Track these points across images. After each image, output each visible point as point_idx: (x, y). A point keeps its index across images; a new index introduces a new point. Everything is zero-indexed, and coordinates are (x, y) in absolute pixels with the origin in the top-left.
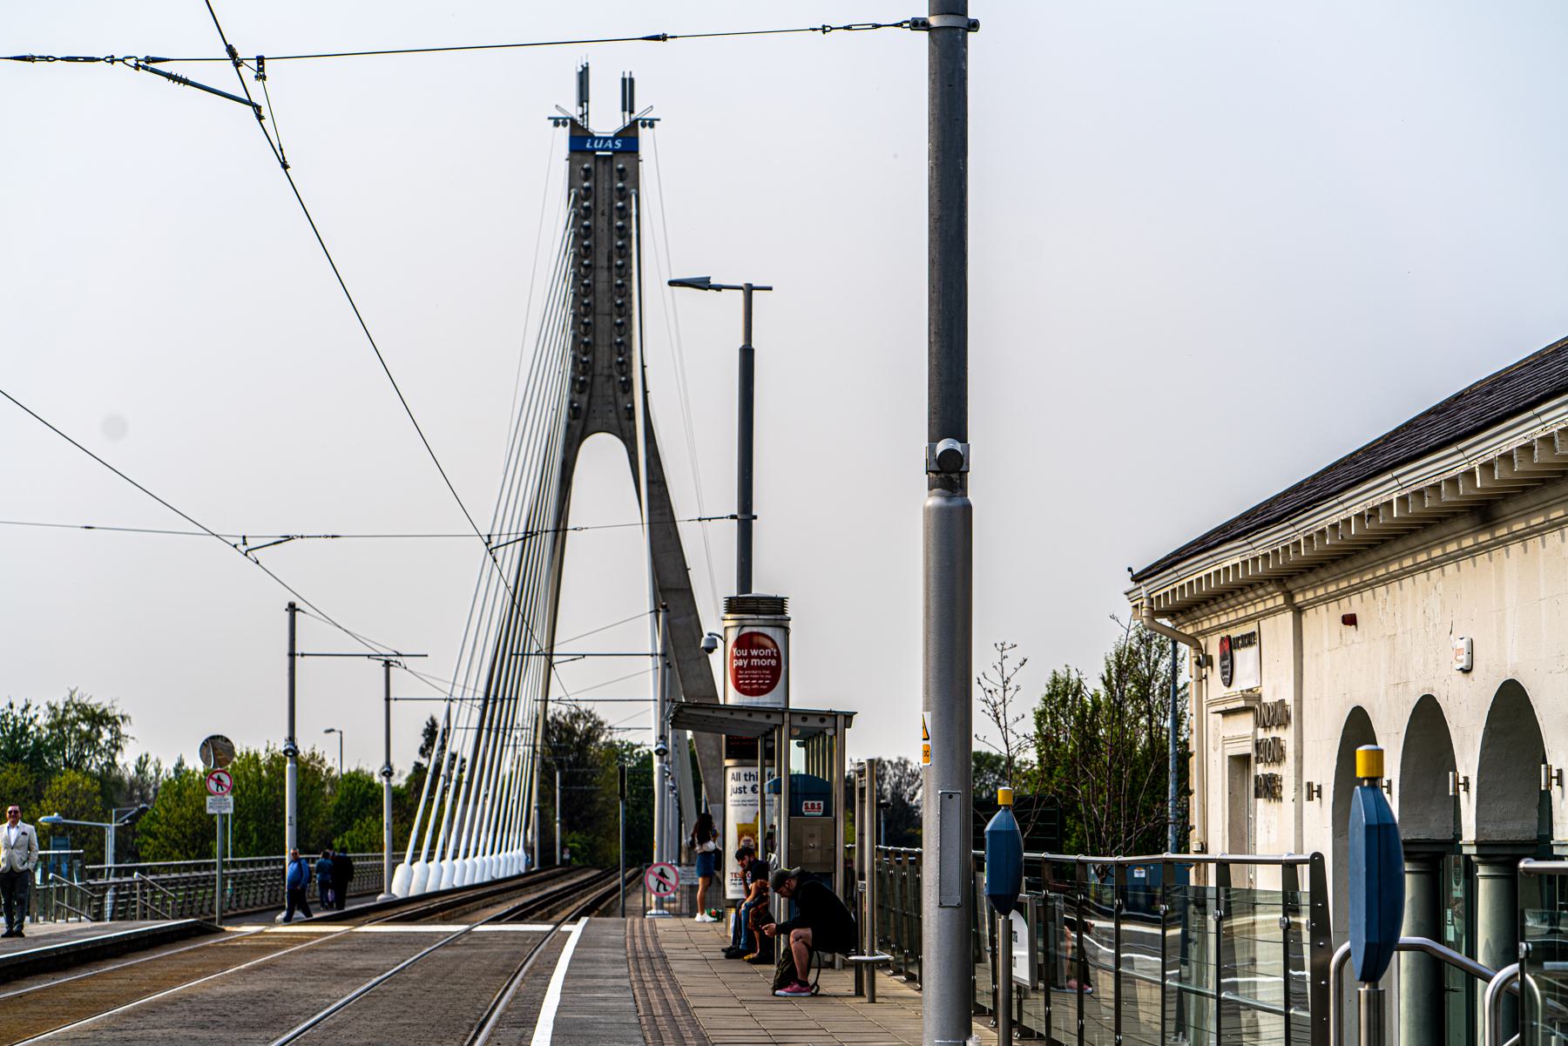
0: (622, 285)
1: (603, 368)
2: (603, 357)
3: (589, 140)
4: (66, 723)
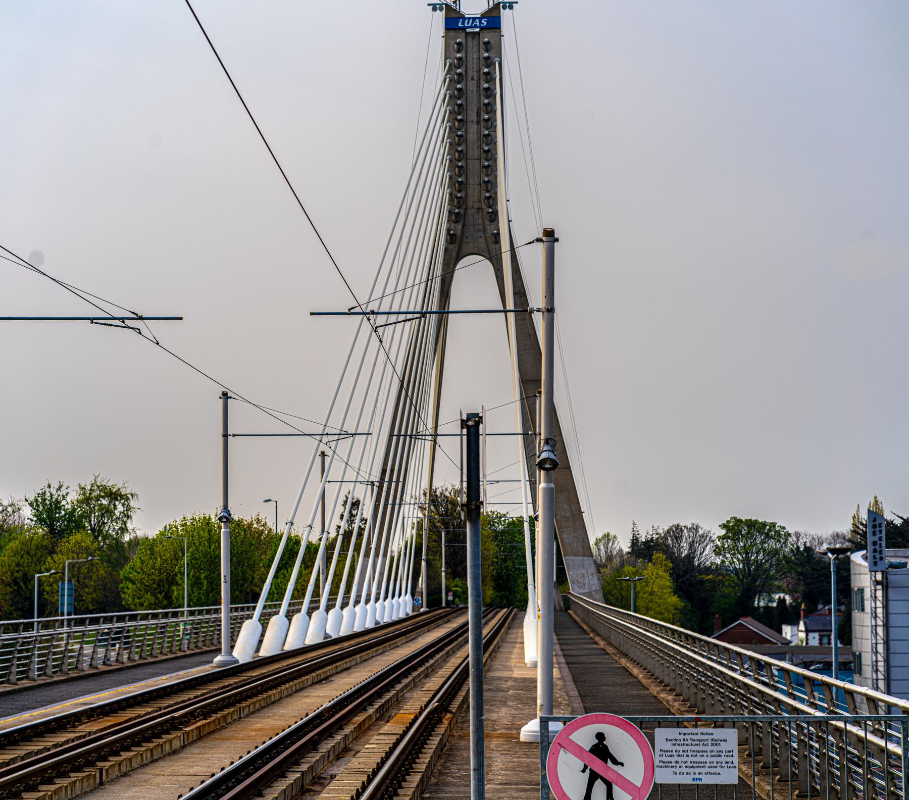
0: (489, 135)
2: (474, 194)
3: (461, 20)
4: (91, 499)
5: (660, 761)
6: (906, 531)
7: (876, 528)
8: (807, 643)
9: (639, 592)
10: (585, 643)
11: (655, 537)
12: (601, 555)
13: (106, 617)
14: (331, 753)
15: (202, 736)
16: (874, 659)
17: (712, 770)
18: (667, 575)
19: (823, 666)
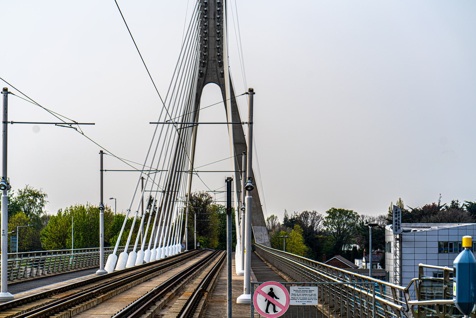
0: (219, 25)
1: (212, 57)
2: (212, 53)
4: (25, 196)
5: (292, 298)
6: (413, 215)
7: (397, 214)
8: (366, 268)
9: (287, 243)
10: (263, 266)
11: (296, 217)
12: (270, 225)
13: (32, 253)
14: (160, 306)
15: (104, 301)
16: (395, 275)
17: (309, 301)
18: (300, 235)
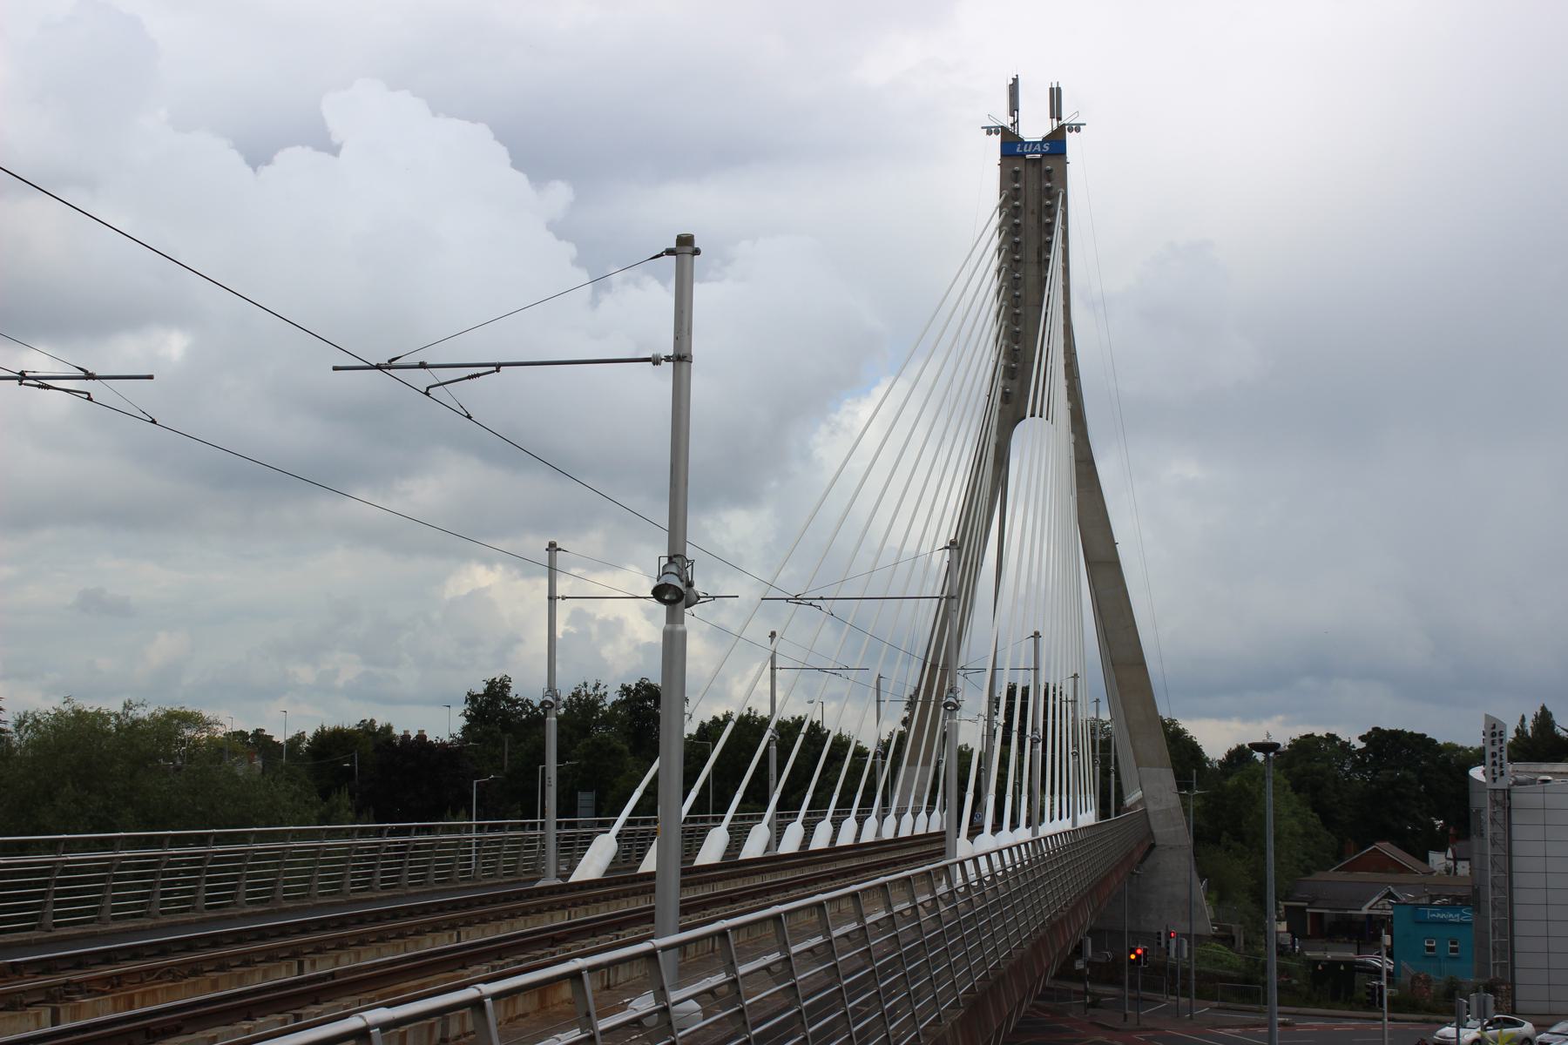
19: (1452, 901)
